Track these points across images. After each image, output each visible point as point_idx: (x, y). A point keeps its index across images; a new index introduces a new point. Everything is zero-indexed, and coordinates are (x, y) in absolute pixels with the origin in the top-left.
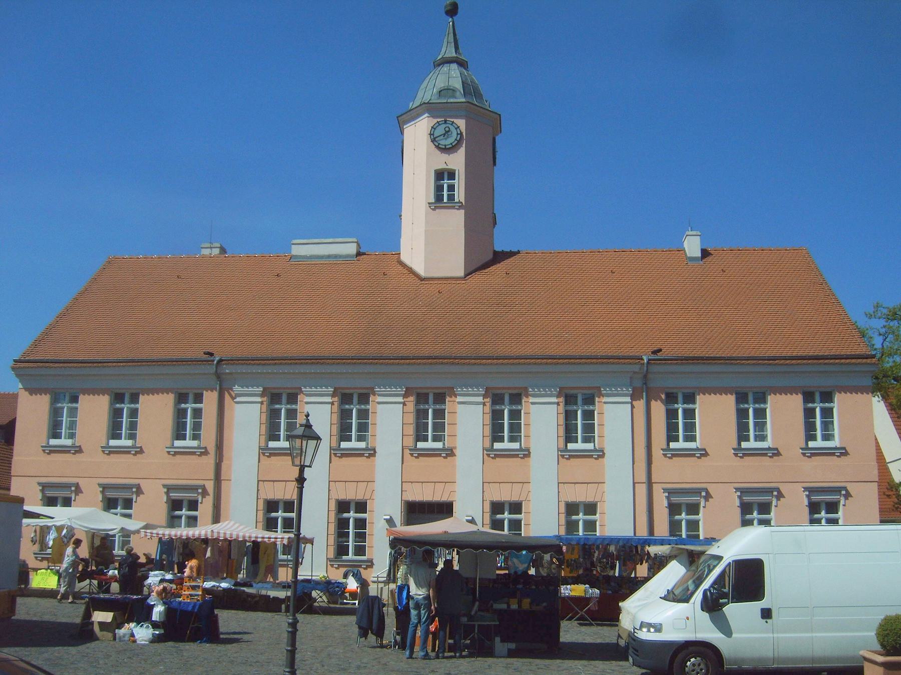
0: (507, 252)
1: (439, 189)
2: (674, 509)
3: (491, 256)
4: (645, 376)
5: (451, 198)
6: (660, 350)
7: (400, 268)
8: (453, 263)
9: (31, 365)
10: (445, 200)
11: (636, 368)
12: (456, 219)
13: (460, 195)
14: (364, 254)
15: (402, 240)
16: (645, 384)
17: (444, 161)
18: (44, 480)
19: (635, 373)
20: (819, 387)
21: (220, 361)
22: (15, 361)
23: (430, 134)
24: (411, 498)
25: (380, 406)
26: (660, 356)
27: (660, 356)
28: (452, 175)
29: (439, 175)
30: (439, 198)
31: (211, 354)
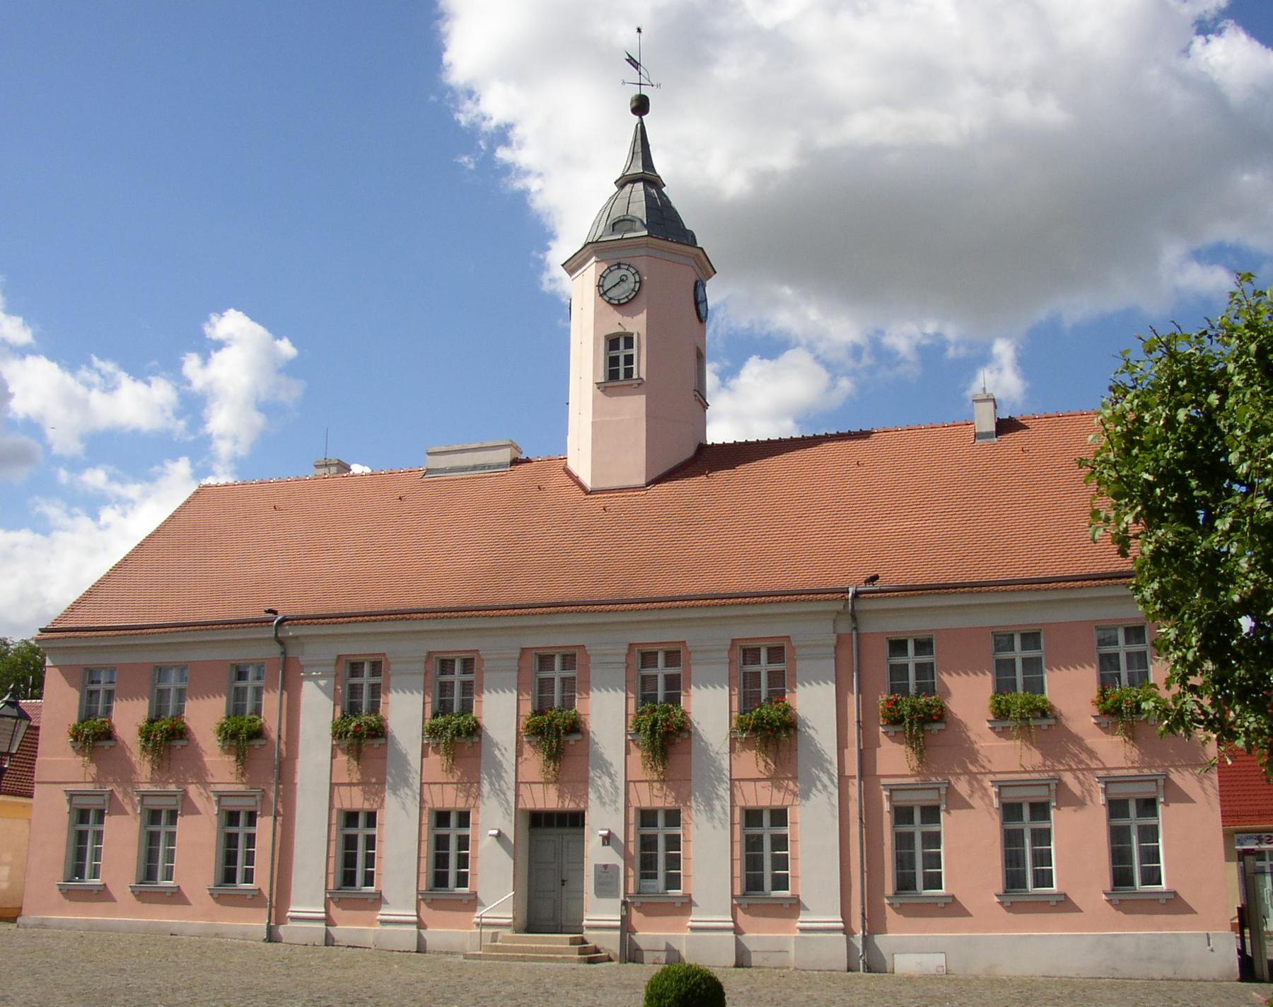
0: (809, 438)
1: (613, 361)
2: (902, 814)
3: (689, 452)
4: (854, 617)
5: (629, 373)
6: (875, 578)
7: (565, 477)
8: (633, 469)
9: (59, 635)
10: (622, 376)
11: (839, 606)
12: (634, 407)
13: (641, 368)
14: (528, 461)
15: (569, 438)
16: (855, 628)
17: (617, 322)
18: (71, 788)
19: (838, 613)
20: (1122, 620)
21: (281, 622)
22: (43, 631)
23: (599, 286)
24: (530, 805)
25: (908, 772)
26: (878, 585)
27: (878, 585)
28: (629, 341)
29: (613, 342)
30: (613, 375)
31: (275, 613)
